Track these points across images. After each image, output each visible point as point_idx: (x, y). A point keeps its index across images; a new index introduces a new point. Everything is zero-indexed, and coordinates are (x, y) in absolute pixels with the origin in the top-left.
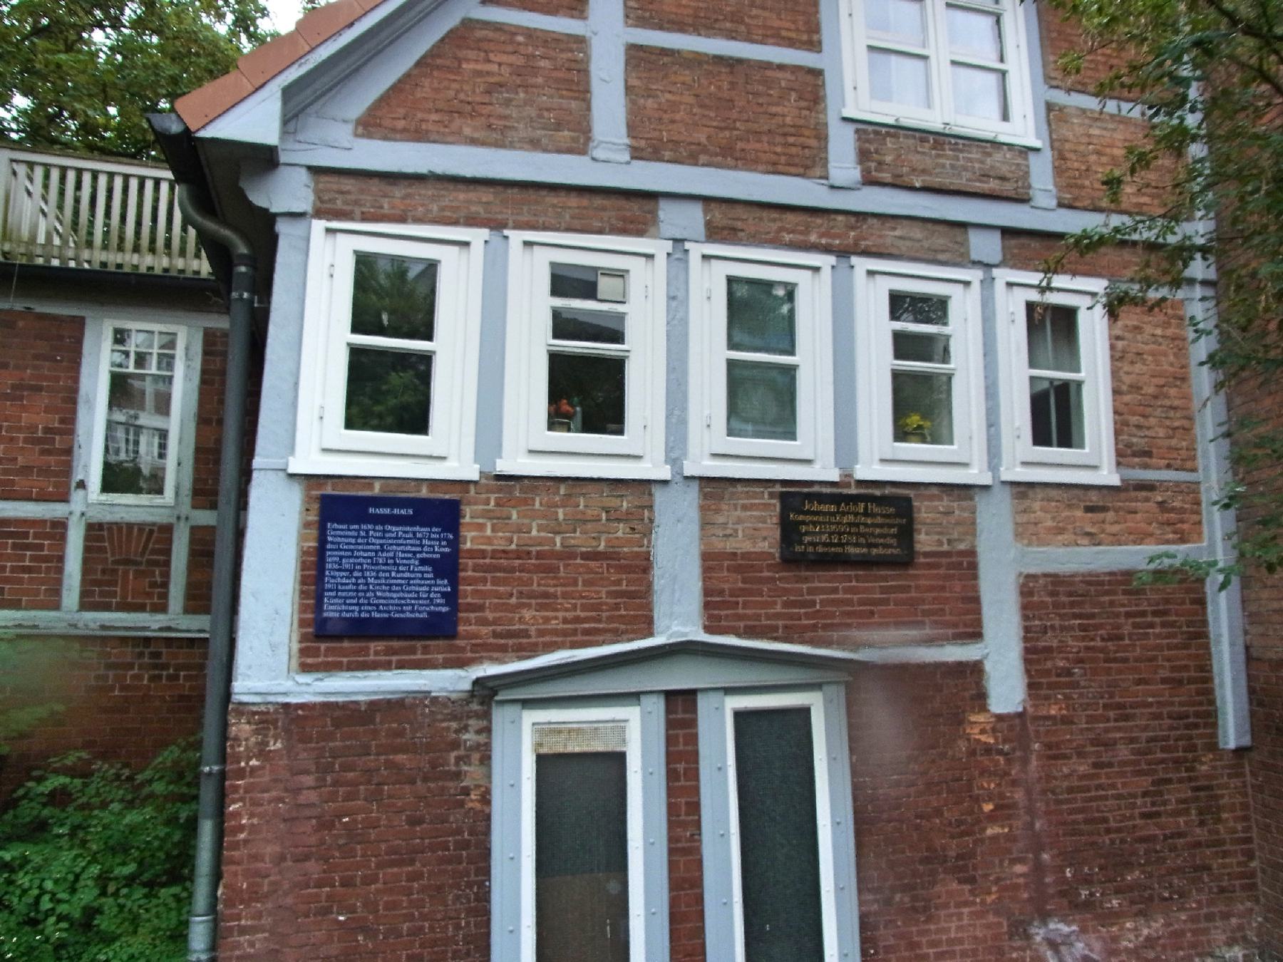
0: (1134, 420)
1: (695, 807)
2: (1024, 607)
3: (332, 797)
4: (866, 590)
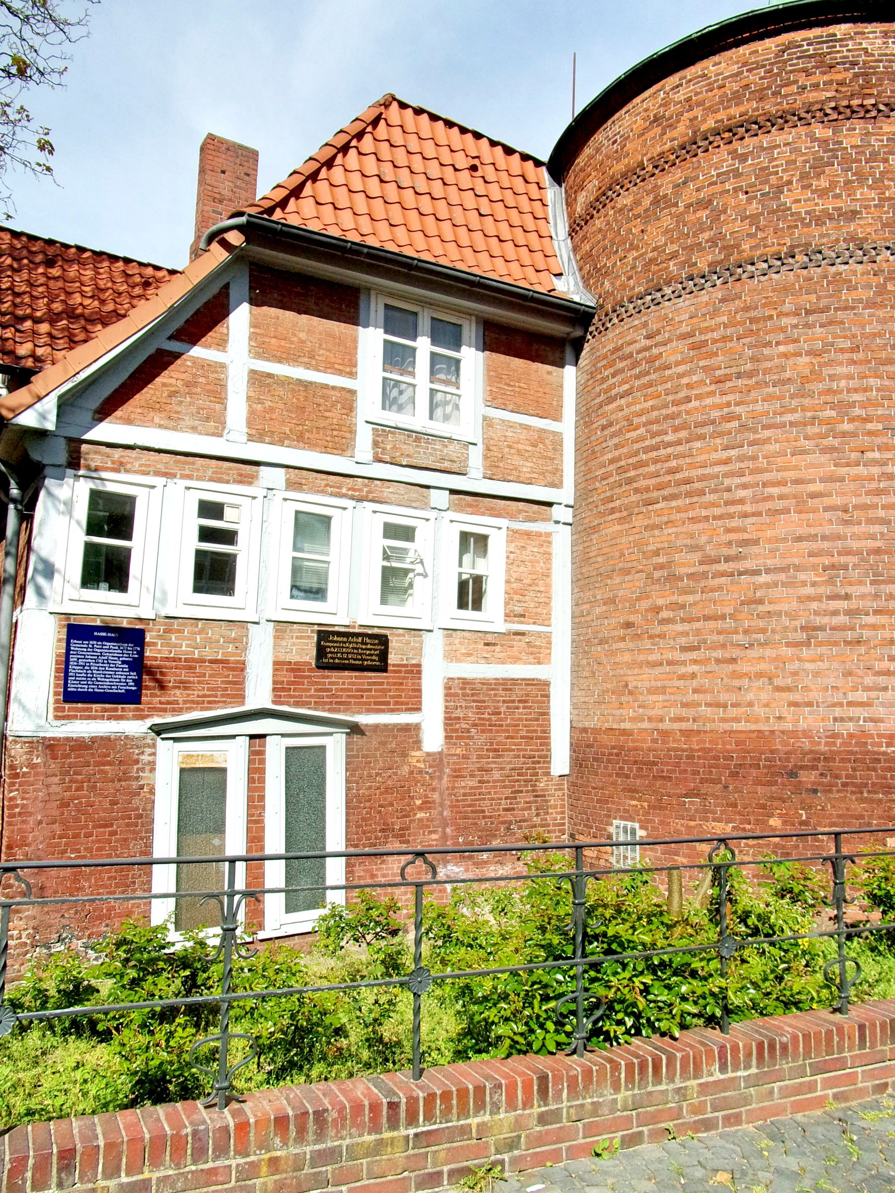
0: (516, 597)
1: (262, 798)
2: (446, 695)
3: (69, 789)
4: (360, 684)
